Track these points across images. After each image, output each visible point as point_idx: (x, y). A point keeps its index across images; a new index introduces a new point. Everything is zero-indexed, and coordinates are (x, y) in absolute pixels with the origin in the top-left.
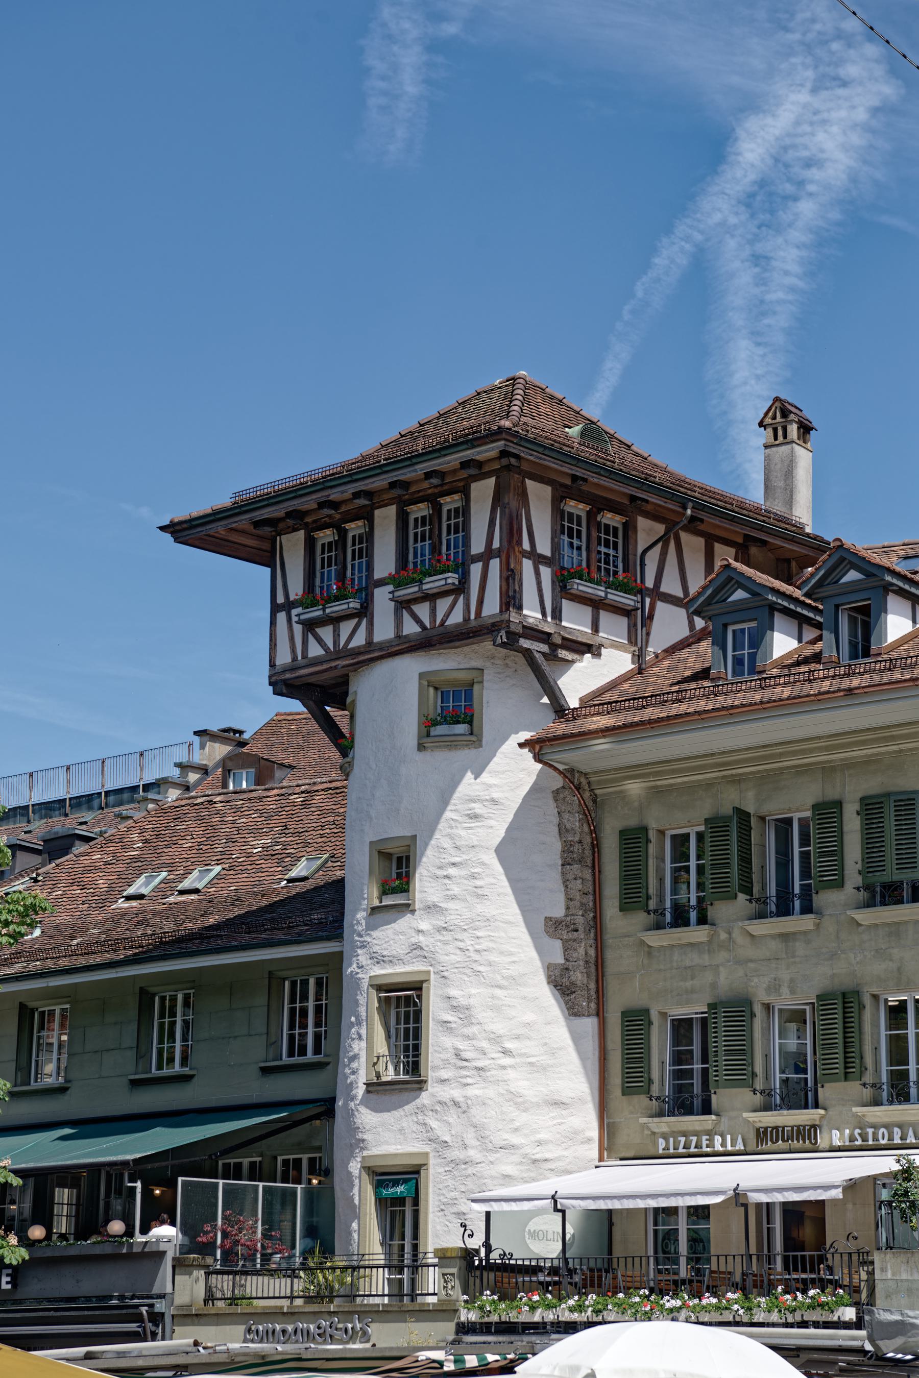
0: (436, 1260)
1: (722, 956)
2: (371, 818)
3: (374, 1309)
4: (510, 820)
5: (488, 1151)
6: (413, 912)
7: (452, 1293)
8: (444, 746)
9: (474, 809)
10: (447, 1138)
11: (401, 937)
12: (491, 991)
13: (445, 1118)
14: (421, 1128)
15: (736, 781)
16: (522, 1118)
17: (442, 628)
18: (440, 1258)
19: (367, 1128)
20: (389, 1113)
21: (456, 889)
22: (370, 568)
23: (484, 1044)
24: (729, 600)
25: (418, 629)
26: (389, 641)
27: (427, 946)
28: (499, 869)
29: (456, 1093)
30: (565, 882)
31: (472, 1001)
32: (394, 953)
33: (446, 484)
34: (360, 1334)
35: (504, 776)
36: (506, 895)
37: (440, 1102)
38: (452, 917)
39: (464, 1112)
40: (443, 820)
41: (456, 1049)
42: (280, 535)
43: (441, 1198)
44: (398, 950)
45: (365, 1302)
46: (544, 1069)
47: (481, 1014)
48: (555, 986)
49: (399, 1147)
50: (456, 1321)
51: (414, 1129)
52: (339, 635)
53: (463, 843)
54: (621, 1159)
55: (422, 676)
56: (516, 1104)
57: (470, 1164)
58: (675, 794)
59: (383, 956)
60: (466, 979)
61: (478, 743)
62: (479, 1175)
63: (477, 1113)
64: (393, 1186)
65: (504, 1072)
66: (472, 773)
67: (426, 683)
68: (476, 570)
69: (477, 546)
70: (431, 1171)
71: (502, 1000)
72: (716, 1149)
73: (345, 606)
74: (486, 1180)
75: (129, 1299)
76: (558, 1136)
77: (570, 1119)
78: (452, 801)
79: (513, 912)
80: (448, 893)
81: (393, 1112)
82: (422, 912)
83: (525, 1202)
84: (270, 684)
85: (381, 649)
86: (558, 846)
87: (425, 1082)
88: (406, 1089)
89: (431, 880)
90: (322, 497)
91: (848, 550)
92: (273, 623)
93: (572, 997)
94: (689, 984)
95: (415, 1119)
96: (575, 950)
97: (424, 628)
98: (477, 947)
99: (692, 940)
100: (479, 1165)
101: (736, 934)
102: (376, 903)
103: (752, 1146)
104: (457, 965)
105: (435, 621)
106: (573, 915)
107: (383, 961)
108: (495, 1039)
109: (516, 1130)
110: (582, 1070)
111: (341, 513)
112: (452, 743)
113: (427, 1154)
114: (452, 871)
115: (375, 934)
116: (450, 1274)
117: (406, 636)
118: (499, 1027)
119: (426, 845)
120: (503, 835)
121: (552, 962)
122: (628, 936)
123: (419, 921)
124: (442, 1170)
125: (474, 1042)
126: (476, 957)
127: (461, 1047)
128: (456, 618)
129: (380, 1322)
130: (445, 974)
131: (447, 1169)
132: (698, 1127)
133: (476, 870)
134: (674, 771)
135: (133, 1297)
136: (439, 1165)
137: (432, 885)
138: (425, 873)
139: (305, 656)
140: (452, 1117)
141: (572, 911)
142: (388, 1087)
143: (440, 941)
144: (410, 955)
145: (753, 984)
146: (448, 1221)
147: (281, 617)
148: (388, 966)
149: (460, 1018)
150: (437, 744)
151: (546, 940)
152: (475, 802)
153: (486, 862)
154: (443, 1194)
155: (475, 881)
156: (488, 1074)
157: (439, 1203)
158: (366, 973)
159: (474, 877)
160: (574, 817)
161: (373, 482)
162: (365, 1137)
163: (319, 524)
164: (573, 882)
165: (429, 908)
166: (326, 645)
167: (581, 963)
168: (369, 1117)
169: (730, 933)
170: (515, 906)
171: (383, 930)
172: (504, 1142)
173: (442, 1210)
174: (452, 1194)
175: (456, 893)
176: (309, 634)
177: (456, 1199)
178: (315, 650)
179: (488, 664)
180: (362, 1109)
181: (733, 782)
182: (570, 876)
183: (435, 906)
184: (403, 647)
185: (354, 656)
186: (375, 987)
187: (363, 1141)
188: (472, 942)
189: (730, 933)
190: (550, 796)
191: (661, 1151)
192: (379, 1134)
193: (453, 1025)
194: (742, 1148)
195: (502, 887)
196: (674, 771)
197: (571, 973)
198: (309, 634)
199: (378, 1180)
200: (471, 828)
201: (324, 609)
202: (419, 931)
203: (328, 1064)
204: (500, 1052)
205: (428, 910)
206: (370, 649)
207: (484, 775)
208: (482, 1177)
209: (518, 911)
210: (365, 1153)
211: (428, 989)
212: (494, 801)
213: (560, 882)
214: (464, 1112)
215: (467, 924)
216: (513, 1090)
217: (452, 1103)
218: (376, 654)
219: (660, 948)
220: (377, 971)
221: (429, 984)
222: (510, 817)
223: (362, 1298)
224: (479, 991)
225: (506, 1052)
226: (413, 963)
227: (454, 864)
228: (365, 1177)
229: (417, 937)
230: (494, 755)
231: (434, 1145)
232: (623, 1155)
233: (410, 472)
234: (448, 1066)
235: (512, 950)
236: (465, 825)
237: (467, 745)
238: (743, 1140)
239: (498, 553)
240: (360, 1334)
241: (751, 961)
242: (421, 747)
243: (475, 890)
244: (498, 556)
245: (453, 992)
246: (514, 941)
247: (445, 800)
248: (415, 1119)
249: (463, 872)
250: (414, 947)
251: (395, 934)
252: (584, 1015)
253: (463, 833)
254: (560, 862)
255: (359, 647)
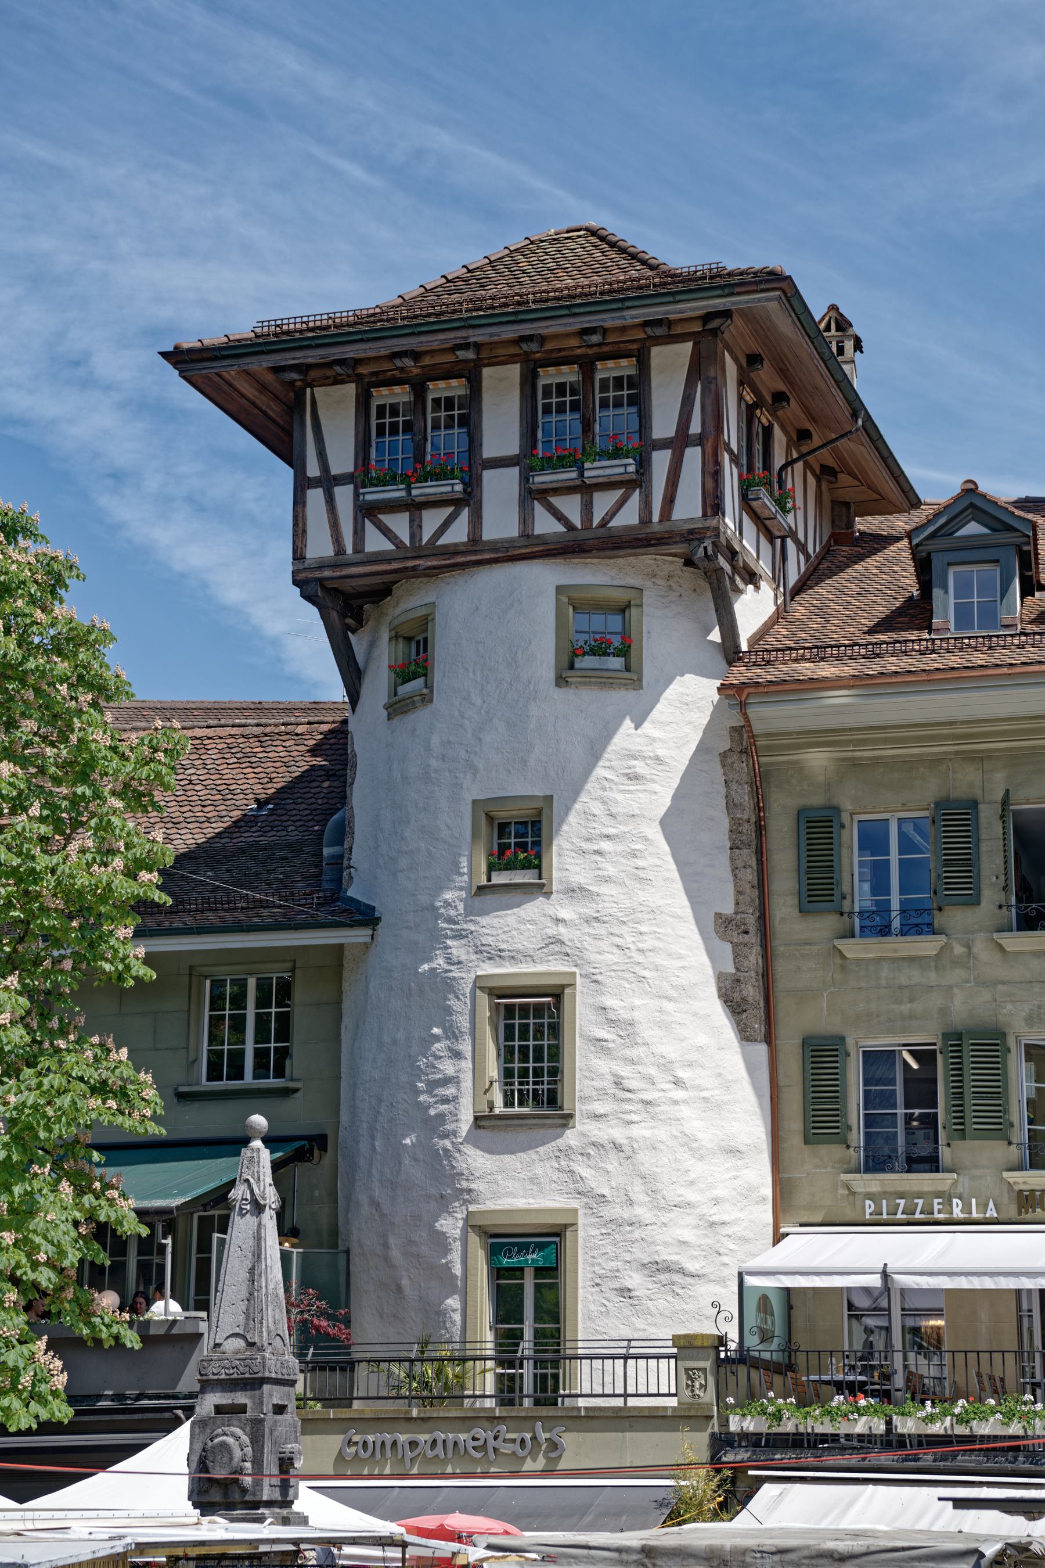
0: (675, 1350)
1: (956, 975)
2: (475, 771)
3: (570, 1414)
4: (676, 785)
5: (660, 1209)
6: (548, 894)
7: (702, 1394)
8: (596, 683)
9: (634, 767)
10: (605, 1191)
11: (529, 927)
12: (657, 1002)
13: (601, 1165)
14: (565, 1177)
15: (978, 758)
16: (697, 1169)
17: (602, 530)
18: (679, 1348)
19: (477, 1174)
20: (513, 1156)
21: (611, 869)
22: (474, 442)
23: (653, 1071)
24: (958, 534)
25: (560, 528)
26: (511, 541)
27: (571, 940)
28: (664, 847)
29: (618, 1134)
30: (734, 869)
31: (637, 1015)
32: (519, 947)
33: (607, 344)
34: (543, 1447)
35: (668, 728)
36: (672, 881)
37: (594, 1144)
38: (606, 905)
39: (629, 1158)
40: (592, 778)
41: (616, 1075)
42: (312, 387)
43: (596, 1268)
44: (525, 943)
45: (478, 1405)
46: (719, 1106)
47: (646, 1032)
48: (725, 1002)
49: (531, 1201)
50: (709, 1430)
51: (555, 1178)
52: (421, 527)
53: (620, 810)
54: (802, 1225)
55: (560, 589)
56: (691, 1149)
57: (637, 1225)
58: (881, 770)
59: (500, 950)
60: (627, 986)
61: (637, 683)
62: (649, 1240)
63: (645, 1160)
64: (519, 1252)
65: (677, 1108)
66: (632, 721)
67: (566, 600)
68: (661, 461)
69: (663, 426)
70: (581, 1233)
71: (672, 1016)
72: (955, 1216)
73: (449, 489)
74: (658, 1248)
75: (131, 1399)
76: (734, 1193)
77: (745, 1171)
78: (606, 755)
79: (681, 903)
80: (601, 873)
81: (518, 1155)
82: (562, 896)
83: (835, 1277)
84: (296, 583)
85: (495, 550)
86: (725, 823)
87: (571, 1116)
88: (543, 1126)
89: (574, 855)
90: (456, 338)
91: (984, 496)
92: (299, 502)
93: (744, 1016)
94: (906, 1008)
95: (557, 1166)
96: (746, 957)
97: (570, 527)
98: (641, 945)
99: (913, 953)
100: (649, 1227)
101: (980, 947)
102: (483, 881)
103: (1012, 1212)
104: (614, 968)
105: (591, 520)
106: (743, 913)
107: (500, 957)
108: (666, 1065)
109: (692, 1183)
110: (758, 1110)
111: (421, 367)
112: (604, 680)
113: (575, 1211)
114: (605, 845)
115: (484, 920)
116: (699, 1369)
117: (539, 536)
118: (670, 1050)
119: (568, 809)
120: (669, 804)
121: (723, 971)
122: (810, 944)
123: (558, 907)
124: (598, 1232)
125: (640, 1068)
126: (640, 958)
127: (623, 1074)
128: (629, 516)
129: (578, 1431)
130: (599, 978)
131: (604, 1231)
132: (927, 1187)
133: (637, 847)
134: (886, 741)
135: (139, 1398)
136: (592, 1225)
137: (577, 862)
138: (566, 845)
139: (359, 547)
140: (612, 1164)
141: (742, 908)
142: (516, 1122)
143: (589, 935)
144: (545, 950)
145: (1005, 1011)
146: (606, 1299)
147: (315, 497)
148: (507, 964)
149: (621, 1036)
150: (603, 680)
151: (717, 942)
152: (634, 757)
153: (650, 836)
154: (599, 1264)
155: (635, 860)
156: (657, 1109)
157: (594, 1275)
158: (469, 972)
159: (634, 854)
160: (743, 789)
161: (547, 327)
162: (473, 1186)
163: (381, 377)
164: (743, 870)
165: (573, 891)
166: (397, 537)
167: (753, 974)
168: (481, 1160)
169: (969, 948)
170: (684, 897)
171: (498, 916)
172: (680, 1199)
173: (598, 1285)
174: (613, 1264)
175: (611, 873)
176: (367, 521)
177: (618, 1271)
178: (375, 542)
179: (648, 583)
180: (469, 1150)
181: (972, 759)
182: (740, 864)
183: (581, 889)
184: (534, 550)
185: (447, 556)
186: (487, 990)
187: (470, 1191)
188: (634, 939)
189: (969, 948)
190: (718, 759)
191: (868, 1217)
192: (496, 1182)
193: (611, 1045)
194: (995, 1215)
195: (668, 870)
196: (886, 741)
197: (743, 986)
198: (367, 521)
199: (492, 1244)
200: (630, 792)
201: (409, 490)
202: (558, 921)
203: (296, 1090)
204: (671, 1082)
205: (571, 894)
206: (475, 548)
207: (646, 724)
208: (653, 1243)
209: (687, 903)
210: (472, 1208)
211: (574, 996)
212: (658, 759)
213: (729, 869)
214: (629, 1158)
215: (627, 915)
216: (687, 1132)
217: (612, 1145)
218: (487, 556)
219: (859, 961)
220: (488, 969)
221: (575, 989)
222: (676, 783)
223: (472, 1400)
224: (643, 1002)
225: (678, 1083)
226: (549, 961)
227: (607, 836)
228: (474, 1239)
229: (555, 928)
230: (658, 701)
231: (586, 1200)
232: (804, 1220)
233: (613, 319)
234: (604, 1097)
235: (681, 951)
236: (622, 787)
237: (625, 685)
238: (995, 1205)
239: (700, 440)
240: (543, 1447)
241: (1003, 983)
242: (561, 681)
243: (636, 871)
244: (700, 445)
245: (609, 1002)
246: (682, 940)
247: (595, 752)
248: (557, 1166)
249: (620, 848)
250: (550, 940)
251: (519, 922)
252: (756, 1041)
253: (620, 797)
254: (728, 845)
255: (456, 545)
